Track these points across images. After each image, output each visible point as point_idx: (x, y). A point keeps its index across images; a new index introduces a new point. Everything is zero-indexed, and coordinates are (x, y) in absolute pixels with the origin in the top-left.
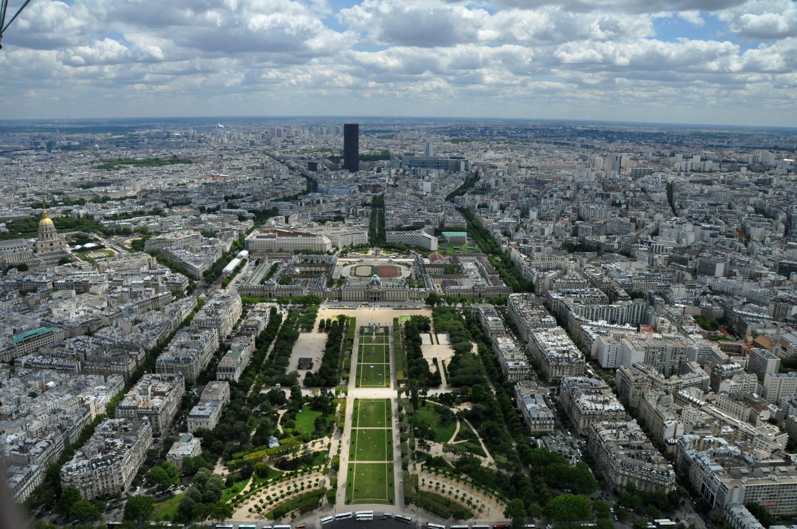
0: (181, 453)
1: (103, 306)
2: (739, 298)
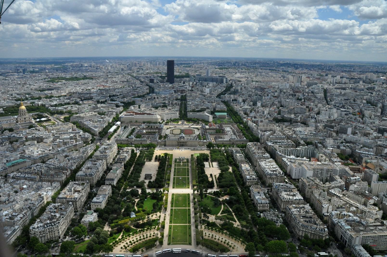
0: (88, 220)
1: (50, 149)
2: (359, 145)
